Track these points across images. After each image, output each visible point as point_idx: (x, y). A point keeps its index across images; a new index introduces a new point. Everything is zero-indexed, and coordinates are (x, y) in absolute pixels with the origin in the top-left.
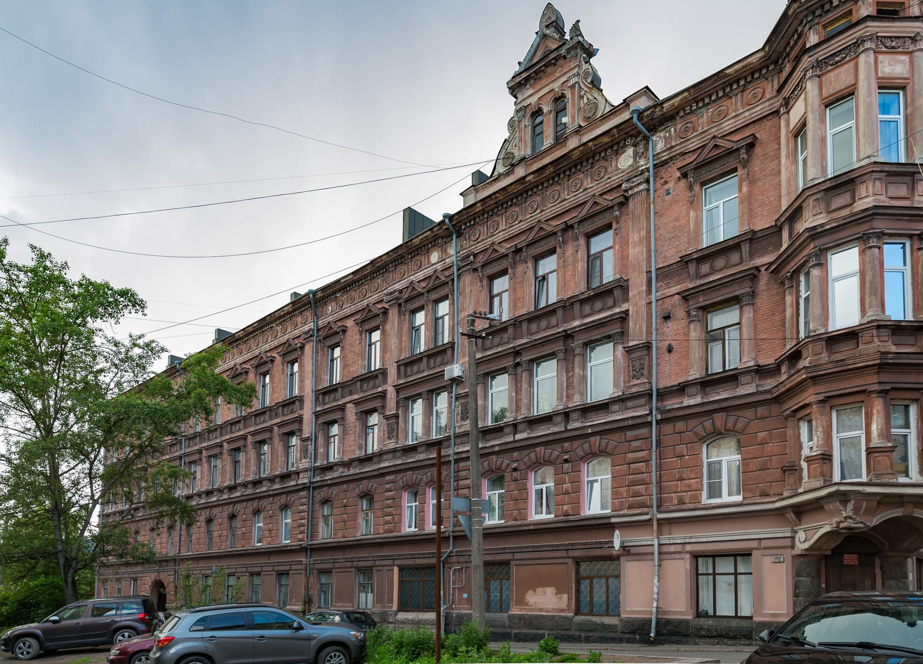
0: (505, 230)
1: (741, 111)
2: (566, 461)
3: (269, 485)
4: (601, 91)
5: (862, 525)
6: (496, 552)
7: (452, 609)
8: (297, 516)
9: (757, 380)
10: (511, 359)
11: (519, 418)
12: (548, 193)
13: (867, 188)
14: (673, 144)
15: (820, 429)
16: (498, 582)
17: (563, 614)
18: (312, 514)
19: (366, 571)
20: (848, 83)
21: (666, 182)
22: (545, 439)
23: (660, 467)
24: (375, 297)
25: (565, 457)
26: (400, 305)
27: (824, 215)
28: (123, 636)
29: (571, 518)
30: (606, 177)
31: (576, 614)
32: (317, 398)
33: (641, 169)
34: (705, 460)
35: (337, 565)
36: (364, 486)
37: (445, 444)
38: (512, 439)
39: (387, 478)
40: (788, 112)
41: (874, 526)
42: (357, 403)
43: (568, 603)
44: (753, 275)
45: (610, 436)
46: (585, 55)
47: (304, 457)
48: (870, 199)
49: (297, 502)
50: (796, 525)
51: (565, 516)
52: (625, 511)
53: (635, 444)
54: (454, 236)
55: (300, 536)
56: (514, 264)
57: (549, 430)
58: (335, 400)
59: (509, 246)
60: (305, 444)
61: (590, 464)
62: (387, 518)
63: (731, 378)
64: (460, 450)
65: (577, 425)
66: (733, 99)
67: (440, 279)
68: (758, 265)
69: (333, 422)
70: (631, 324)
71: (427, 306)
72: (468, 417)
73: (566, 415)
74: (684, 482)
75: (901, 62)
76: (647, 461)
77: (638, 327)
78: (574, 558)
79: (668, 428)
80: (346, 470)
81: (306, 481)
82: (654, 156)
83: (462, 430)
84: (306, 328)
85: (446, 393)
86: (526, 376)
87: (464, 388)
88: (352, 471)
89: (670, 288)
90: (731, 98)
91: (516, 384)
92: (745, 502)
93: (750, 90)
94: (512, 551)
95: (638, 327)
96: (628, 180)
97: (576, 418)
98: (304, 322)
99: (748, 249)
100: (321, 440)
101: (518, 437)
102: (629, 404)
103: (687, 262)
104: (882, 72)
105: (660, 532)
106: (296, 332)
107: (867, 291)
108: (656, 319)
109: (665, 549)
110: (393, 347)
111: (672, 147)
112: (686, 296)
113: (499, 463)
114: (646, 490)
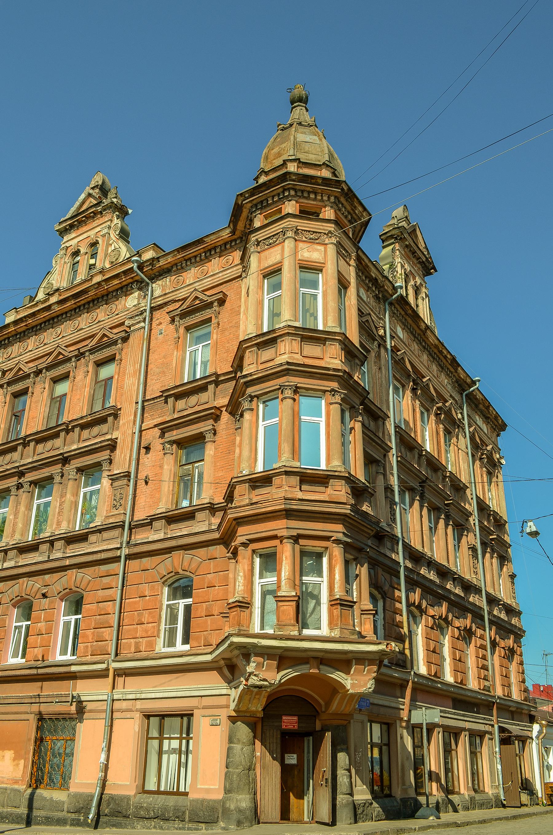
0: (31, 351)
1: (217, 271)
5: (266, 683)
13: (285, 346)
21: (161, 323)
30: (116, 313)
34: (165, 603)
38: (296, 633)
46: (117, 213)
52: (89, 658)
65: (59, 555)
75: (317, 250)
97: (59, 548)
103: (167, 397)
109: (117, 705)
111: (165, 294)
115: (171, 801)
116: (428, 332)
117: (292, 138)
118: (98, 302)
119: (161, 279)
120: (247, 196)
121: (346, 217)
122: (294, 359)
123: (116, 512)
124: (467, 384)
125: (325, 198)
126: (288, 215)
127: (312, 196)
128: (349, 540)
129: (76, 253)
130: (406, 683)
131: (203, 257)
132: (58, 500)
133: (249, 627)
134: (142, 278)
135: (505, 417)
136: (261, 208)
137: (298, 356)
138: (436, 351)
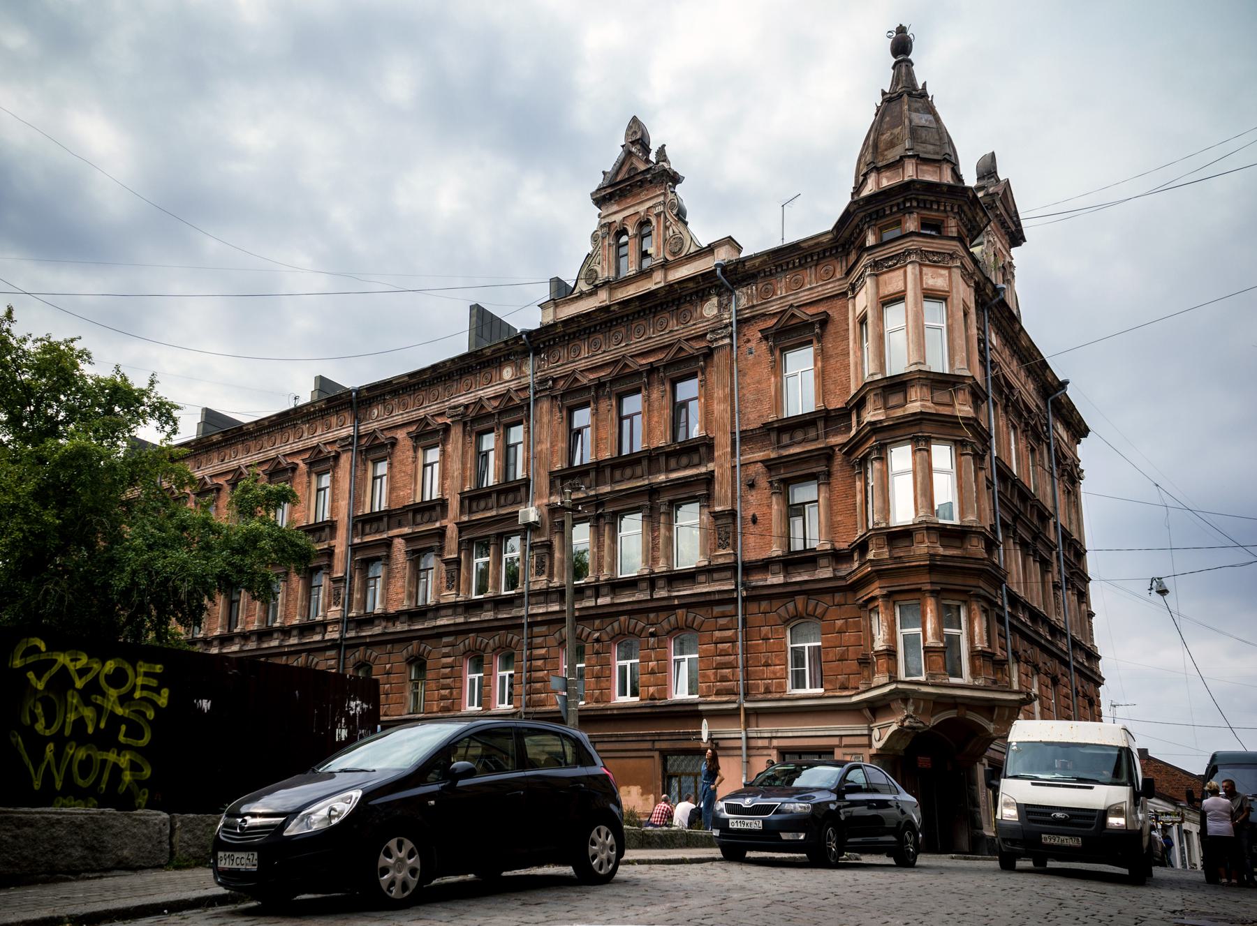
2: (652, 635)
3: (282, 638)
4: (686, 224)
5: (921, 725)
11: (601, 579)
12: (633, 326)
13: (916, 392)
14: (755, 303)
15: (885, 624)
21: (749, 341)
22: (629, 607)
23: (746, 650)
24: (434, 408)
25: (652, 630)
26: (465, 424)
29: (658, 703)
30: (692, 323)
32: (355, 526)
34: (790, 646)
36: (413, 648)
39: (445, 640)
42: (408, 538)
45: (697, 610)
47: (335, 603)
48: (918, 404)
51: (651, 699)
52: (713, 698)
53: (722, 621)
57: (634, 596)
62: (443, 692)
63: (809, 559)
64: (534, 611)
66: (808, 271)
70: (716, 487)
71: (498, 429)
72: (453, 586)
75: (942, 275)
79: (753, 607)
80: (390, 624)
82: (737, 311)
83: (537, 587)
87: (540, 536)
90: (806, 269)
91: (598, 538)
92: (826, 695)
96: (713, 331)
97: (662, 586)
98: (340, 424)
101: (601, 601)
102: (716, 576)
104: (926, 283)
105: (747, 725)
106: (330, 436)
109: (753, 743)
112: (770, 465)
116: (1022, 334)
118: (667, 306)
120: (861, 203)
121: (966, 226)
124: (1053, 388)
125: (948, 208)
126: (912, 234)
127: (935, 207)
131: (797, 264)
133: (896, 673)
134: (722, 284)
136: (876, 219)
137: (929, 404)
138: (1026, 353)
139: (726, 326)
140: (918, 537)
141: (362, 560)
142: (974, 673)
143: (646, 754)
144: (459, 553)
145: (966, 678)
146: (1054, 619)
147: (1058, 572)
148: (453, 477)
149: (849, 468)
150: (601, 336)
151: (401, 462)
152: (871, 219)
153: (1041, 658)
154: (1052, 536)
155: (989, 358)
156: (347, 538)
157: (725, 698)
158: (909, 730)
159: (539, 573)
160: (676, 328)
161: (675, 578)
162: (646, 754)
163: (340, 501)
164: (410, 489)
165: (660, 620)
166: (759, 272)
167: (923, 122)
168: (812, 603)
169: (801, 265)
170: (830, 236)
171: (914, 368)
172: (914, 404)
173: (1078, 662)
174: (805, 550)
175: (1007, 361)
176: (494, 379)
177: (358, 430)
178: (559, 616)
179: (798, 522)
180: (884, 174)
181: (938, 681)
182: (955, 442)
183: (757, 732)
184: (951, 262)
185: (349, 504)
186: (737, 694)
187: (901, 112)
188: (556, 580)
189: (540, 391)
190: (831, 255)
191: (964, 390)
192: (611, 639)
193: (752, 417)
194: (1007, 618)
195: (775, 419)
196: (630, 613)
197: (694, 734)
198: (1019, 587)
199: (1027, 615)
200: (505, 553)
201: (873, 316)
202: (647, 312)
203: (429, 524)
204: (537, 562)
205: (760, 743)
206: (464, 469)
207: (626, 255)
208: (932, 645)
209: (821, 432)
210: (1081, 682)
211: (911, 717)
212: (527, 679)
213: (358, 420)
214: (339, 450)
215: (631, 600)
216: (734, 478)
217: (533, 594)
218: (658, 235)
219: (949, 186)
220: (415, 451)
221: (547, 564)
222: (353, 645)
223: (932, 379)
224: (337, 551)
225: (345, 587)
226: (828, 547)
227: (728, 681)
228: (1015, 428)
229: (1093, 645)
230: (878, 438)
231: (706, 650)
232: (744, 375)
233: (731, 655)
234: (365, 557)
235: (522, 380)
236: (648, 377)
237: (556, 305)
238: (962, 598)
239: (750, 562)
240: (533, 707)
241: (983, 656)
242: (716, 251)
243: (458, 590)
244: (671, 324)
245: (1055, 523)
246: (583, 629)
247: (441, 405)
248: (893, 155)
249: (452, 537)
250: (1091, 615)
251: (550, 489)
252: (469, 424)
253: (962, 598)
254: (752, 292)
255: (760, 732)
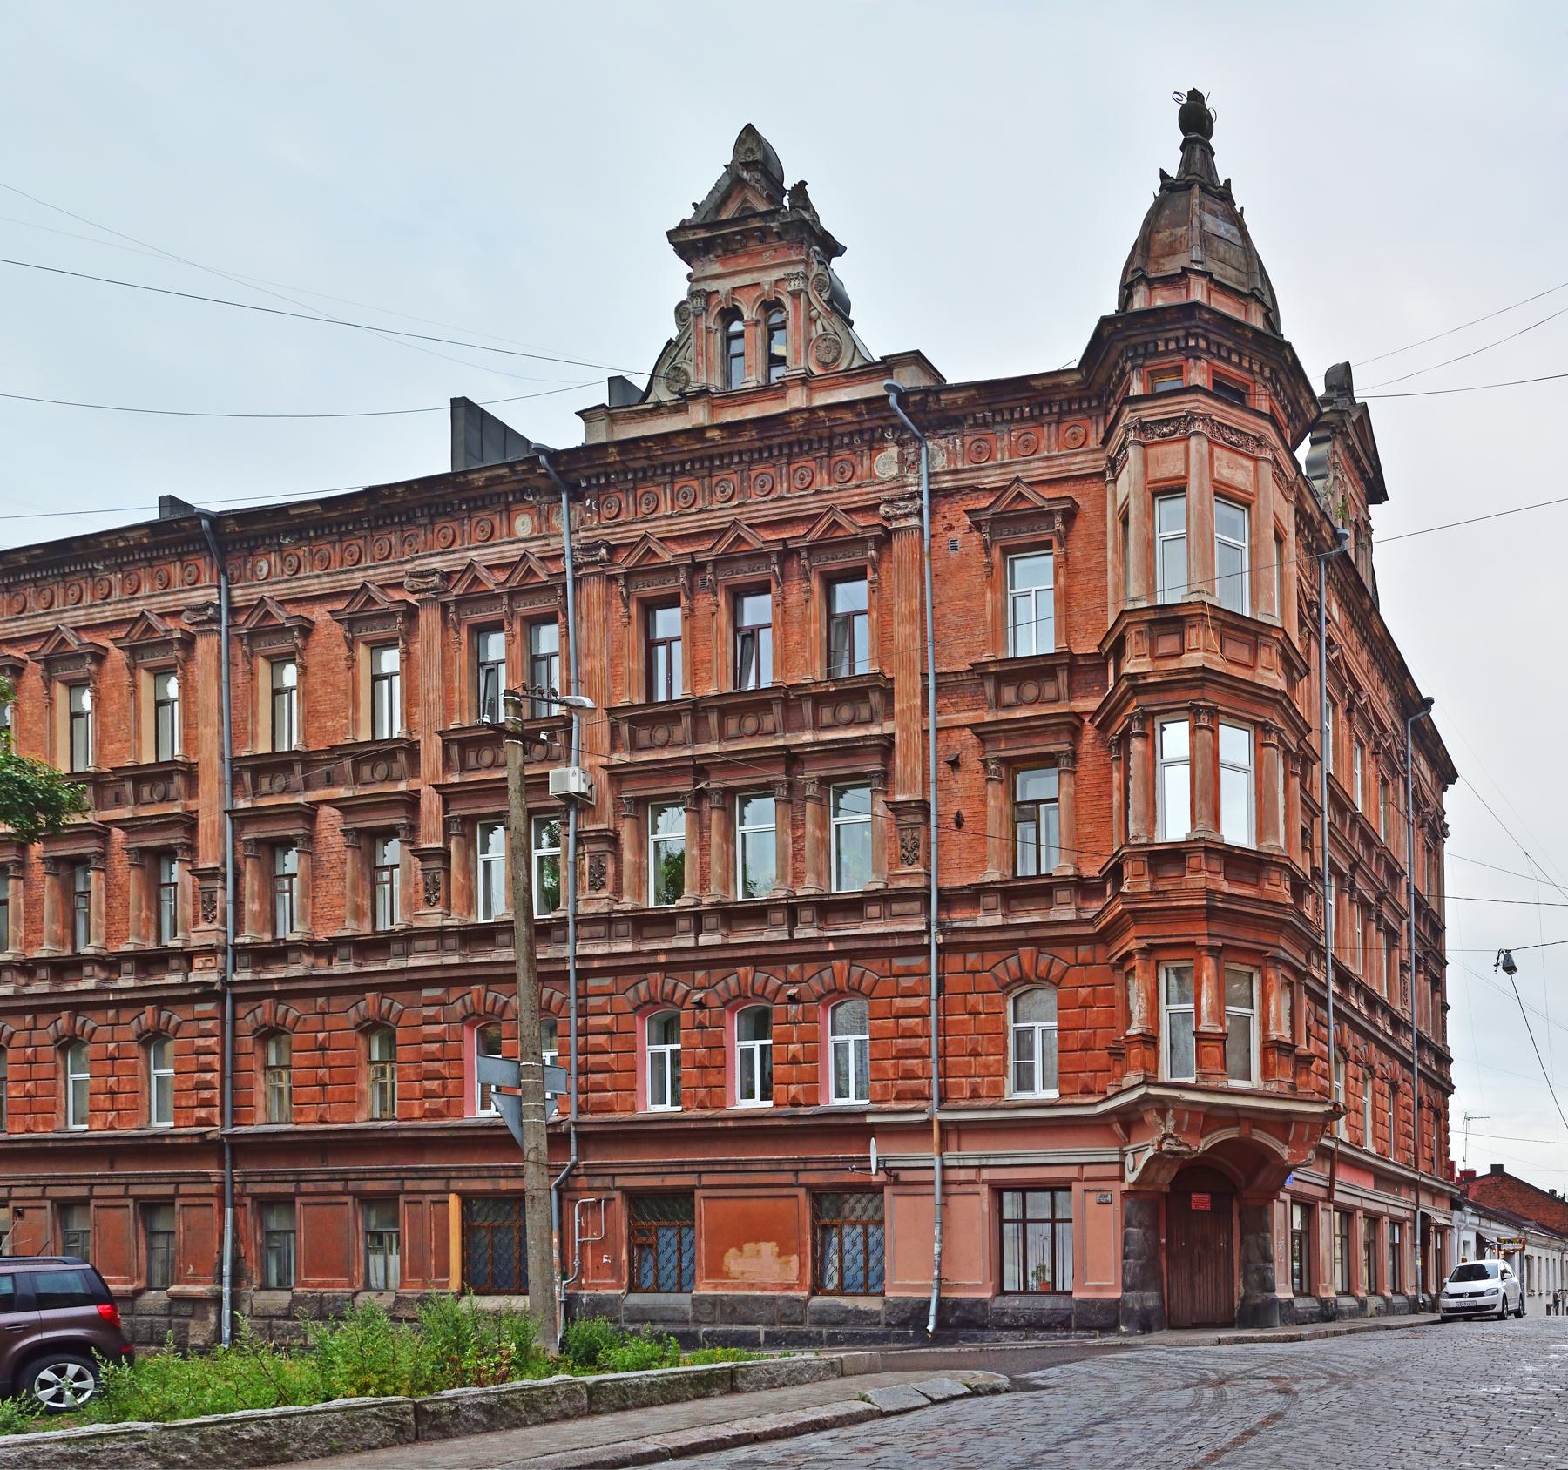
2: (793, 1000)
3: (103, 975)
4: (851, 324)
5: (1186, 1149)
6: (665, 1169)
7: (581, 1287)
8: (192, 1062)
9: (1079, 900)
10: (690, 780)
11: (705, 901)
12: (753, 474)
13: (1197, 637)
14: (960, 466)
15: (1143, 994)
16: (675, 1231)
17: (791, 1293)
18: (234, 1061)
19: (385, 1202)
20: (1175, 473)
21: (950, 528)
22: (753, 952)
23: (943, 1030)
24: (383, 573)
25: (792, 992)
26: (445, 607)
27: (1147, 659)
28: (45, 1384)
29: (802, 1111)
30: (854, 482)
31: (814, 1293)
32: (236, 778)
33: (910, 489)
34: (1011, 1025)
35: (304, 1187)
36: (368, 1004)
37: (557, 934)
39: (426, 993)
40: (1114, 482)
41: (1204, 1152)
42: (346, 807)
43: (800, 1273)
44: (1072, 725)
45: (866, 963)
46: (817, 248)
47: (206, 917)
48: (1200, 654)
49: (190, 1028)
50: (1126, 1145)
51: (793, 1105)
52: (893, 1105)
53: (906, 982)
54: (564, 497)
55: (202, 1113)
56: (692, 591)
57: (762, 934)
58: (285, 790)
59: (680, 551)
60: (206, 884)
61: (840, 1010)
62: (428, 1084)
63: (1042, 890)
64: (588, 951)
65: (811, 932)
66: (1046, 429)
67: (536, 574)
68: (1077, 710)
69: (287, 844)
70: (898, 761)
71: (510, 624)
72: (438, 899)
73: (792, 910)
74: (978, 1058)
75: (1243, 467)
76: (925, 1016)
77: (909, 769)
78: (809, 1187)
79: (954, 962)
80: (323, 961)
81: (212, 977)
82: (930, 475)
83: (591, 909)
84: (198, 597)
85: (501, 828)
86: (719, 819)
87: (594, 821)
88: (337, 968)
89: (958, 712)
90: (1042, 426)
91: (701, 833)
92: (1060, 1102)
93: (1068, 425)
94: (696, 1168)
95: (909, 769)
96: (890, 502)
97: (810, 919)
98: (191, 579)
99: (1065, 679)
100: (250, 882)
101: (704, 940)
102: (896, 908)
104: (1219, 473)
105: (944, 1145)
106: (170, 601)
107: (1197, 793)
108: (937, 764)
109: (952, 1175)
110: (431, 697)
112: (983, 733)
113: (668, 988)
114: (923, 1068)
115: (1048, 1303)
117: (1195, 222)
119: (945, 436)
121: (1284, 408)
122: (1212, 662)
123: (910, 870)
125: (1256, 368)
126: (1196, 389)
127: (1235, 358)
128: (1237, 1303)
129: (731, 314)
130: (1077, 723)
132: (789, 831)
133: (1156, 1072)
135: (839, 238)
138: (1380, 647)
139: (912, 497)
140: (1193, 862)
141: (259, 842)
142: (1266, 1073)
143: (785, 1191)
144: (446, 839)
145: (1256, 1082)
146: (1398, 1008)
147: (1408, 948)
148: (426, 702)
149: (1103, 751)
150: (695, 483)
151: (326, 666)
152: (1136, 356)
153: (1377, 1058)
154: (1403, 901)
155: (1325, 634)
156: (222, 798)
157: (909, 1105)
158: (1169, 1157)
159: (597, 885)
160: (827, 488)
161: (828, 908)
162: (785, 1191)
163: (201, 728)
164: (346, 718)
165: (806, 976)
166: (965, 417)
167: (1221, 232)
168: (1044, 960)
169: (1032, 417)
170: (1077, 377)
171: (1194, 598)
172: (1195, 655)
173: (1424, 1065)
174: (1039, 876)
175: (1354, 648)
176: (497, 533)
177: (229, 597)
178: (509, 970)
179: (1026, 830)
180: (1158, 292)
181: (1212, 1084)
182: (1255, 723)
183: (958, 1158)
184: (1257, 450)
185: (220, 733)
186: (929, 1099)
187: (1188, 206)
188: (626, 899)
189: (587, 564)
190: (1080, 410)
191: (1270, 647)
192: (725, 1004)
193: (958, 651)
194: (1331, 1000)
195: (993, 659)
196: (756, 962)
197: (860, 1160)
198: (1353, 961)
199: (1362, 999)
200: (836, 815)
201: (1137, 508)
202: (775, 452)
203: (387, 783)
204: (591, 867)
205: (963, 1175)
206: (448, 690)
207: (742, 355)
208: (1206, 1030)
209: (1064, 690)
210: (1381, 1058)
211: (1171, 1137)
212: (578, 1066)
213: (227, 576)
214: (192, 630)
215: (758, 939)
216: (925, 749)
217: (582, 921)
218: (797, 328)
219: (1255, 331)
220: (351, 645)
221: (610, 870)
222: (252, 995)
223: (1222, 621)
224: (203, 821)
225: (225, 889)
226: (1070, 872)
227: (915, 1078)
228: (1362, 746)
229: (1445, 1045)
230: (1141, 703)
231: (880, 1028)
232: (944, 583)
233: (920, 1037)
234: (262, 836)
235: (552, 541)
236: (781, 564)
237: (613, 420)
238: (1254, 962)
239: (952, 889)
240: (592, 1113)
241: (1279, 1049)
242: (895, 371)
243: (448, 906)
244: (818, 479)
245: (1408, 885)
246: (552, 995)
247: (396, 568)
248: (1172, 266)
249: (430, 812)
250: (1447, 826)
251: (233, 788)
252: (452, 609)
253: (1254, 962)
254: (954, 447)
255: (963, 1158)
